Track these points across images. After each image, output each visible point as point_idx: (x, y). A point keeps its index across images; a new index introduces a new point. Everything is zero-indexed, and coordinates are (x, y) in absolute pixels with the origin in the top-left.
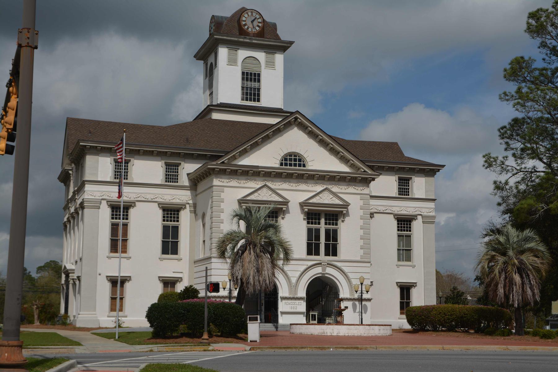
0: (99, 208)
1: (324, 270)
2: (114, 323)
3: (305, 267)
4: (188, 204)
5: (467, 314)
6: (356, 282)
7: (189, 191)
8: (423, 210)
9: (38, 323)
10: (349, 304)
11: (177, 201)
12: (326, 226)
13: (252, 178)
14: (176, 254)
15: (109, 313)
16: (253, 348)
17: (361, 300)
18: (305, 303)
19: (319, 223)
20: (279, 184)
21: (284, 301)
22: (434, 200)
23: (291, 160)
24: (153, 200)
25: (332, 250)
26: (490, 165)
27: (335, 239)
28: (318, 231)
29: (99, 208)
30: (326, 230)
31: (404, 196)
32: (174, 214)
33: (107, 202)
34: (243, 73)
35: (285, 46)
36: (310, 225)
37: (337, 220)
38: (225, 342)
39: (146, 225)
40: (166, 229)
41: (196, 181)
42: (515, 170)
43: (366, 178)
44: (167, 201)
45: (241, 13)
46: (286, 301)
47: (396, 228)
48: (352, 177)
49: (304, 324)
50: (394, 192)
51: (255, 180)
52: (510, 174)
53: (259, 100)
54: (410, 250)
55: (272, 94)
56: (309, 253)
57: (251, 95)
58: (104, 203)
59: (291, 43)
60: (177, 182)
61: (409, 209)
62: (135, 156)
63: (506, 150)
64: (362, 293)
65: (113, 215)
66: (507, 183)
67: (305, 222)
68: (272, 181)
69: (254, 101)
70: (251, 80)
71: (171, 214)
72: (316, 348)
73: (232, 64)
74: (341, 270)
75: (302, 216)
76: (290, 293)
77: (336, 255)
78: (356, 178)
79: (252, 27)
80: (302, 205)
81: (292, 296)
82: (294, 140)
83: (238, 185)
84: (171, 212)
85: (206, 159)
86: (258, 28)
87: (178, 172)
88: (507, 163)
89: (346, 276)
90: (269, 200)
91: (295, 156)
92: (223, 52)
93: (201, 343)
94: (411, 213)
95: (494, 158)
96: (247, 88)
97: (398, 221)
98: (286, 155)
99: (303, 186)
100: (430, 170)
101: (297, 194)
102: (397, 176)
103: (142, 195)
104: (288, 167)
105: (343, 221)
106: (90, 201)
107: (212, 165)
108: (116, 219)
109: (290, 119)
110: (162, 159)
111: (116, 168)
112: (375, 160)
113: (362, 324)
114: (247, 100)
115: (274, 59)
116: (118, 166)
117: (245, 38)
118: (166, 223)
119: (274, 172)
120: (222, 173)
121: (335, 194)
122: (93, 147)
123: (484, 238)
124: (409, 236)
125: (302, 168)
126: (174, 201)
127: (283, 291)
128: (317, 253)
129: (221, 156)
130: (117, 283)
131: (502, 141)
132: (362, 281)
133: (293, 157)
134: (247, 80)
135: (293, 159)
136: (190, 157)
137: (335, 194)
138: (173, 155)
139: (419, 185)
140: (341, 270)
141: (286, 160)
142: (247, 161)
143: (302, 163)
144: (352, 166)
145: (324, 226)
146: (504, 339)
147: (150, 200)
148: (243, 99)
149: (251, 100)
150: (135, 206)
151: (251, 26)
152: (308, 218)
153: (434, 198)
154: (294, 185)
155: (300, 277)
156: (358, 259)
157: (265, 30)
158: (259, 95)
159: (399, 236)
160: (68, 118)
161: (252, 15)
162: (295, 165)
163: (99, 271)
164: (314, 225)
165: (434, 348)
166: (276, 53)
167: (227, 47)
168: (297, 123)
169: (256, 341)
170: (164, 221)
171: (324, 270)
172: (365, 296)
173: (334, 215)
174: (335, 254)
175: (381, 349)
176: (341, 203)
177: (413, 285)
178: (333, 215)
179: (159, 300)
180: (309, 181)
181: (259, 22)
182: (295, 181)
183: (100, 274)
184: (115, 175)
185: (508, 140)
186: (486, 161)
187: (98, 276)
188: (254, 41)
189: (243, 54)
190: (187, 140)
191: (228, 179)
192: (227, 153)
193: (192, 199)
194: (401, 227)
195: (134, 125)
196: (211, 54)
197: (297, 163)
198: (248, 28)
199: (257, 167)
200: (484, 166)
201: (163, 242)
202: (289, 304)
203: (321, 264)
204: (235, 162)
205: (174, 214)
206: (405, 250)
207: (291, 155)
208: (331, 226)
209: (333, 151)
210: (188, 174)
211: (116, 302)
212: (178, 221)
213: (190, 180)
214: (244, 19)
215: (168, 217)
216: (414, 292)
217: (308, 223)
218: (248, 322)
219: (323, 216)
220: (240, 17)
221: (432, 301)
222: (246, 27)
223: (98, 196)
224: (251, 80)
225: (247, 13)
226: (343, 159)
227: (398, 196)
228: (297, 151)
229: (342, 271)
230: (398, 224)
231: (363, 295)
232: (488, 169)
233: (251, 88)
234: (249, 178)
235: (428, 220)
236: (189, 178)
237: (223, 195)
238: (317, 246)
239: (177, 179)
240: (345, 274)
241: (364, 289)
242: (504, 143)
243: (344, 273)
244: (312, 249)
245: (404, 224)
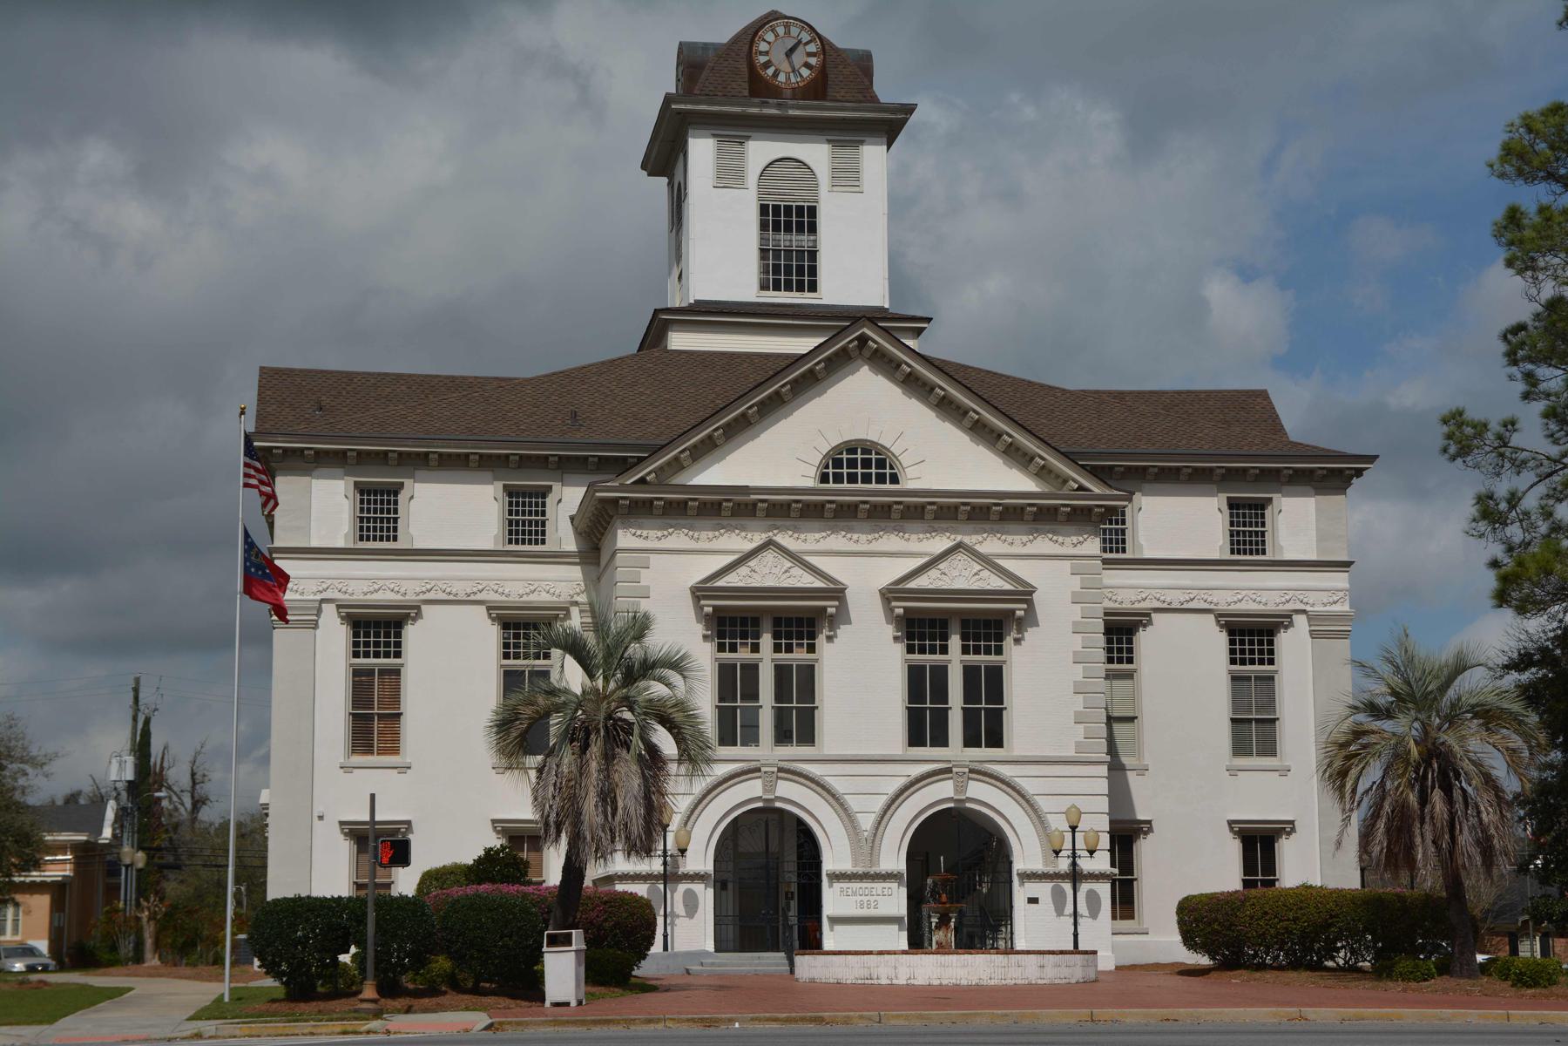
1: (960, 788)
3: (902, 782)
4: (576, 603)
5: (1336, 916)
6: (1059, 824)
7: (578, 568)
8: (1311, 597)
9: (156, 962)
10: (1043, 890)
12: (966, 657)
13: (733, 522)
16: (501, 1023)
17: (1075, 876)
18: (904, 891)
19: (944, 650)
20: (817, 536)
21: (837, 886)
22: (1348, 564)
23: (852, 464)
24: (472, 598)
25: (987, 728)
26: (1464, 451)
27: (996, 693)
28: (941, 673)
29: (316, 627)
30: (965, 668)
33: (339, 607)
34: (764, 209)
35: (891, 120)
36: (971, 657)
37: (1000, 638)
38: (467, 1009)
42: (1546, 462)
43: (1089, 509)
44: (514, 598)
45: (751, 32)
46: (845, 885)
48: (1040, 508)
49: (904, 952)
51: (743, 529)
52: (1528, 477)
53: (813, 287)
54: (1274, 721)
55: (852, 272)
56: (916, 739)
57: (788, 271)
58: (329, 611)
59: (909, 109)
60: (543, 542)
61: (1264, 597)
62: (419, 473)
63: (1526, 396)
64: (1074, 855)
65: (356, 644)
66: (1514, 499)
67: (899, 649)
68: (796, 529)
69: (800, 289)
70: (788, 225)
72: (693, 1020)
74: (1014, 788)
75: (890, 631)
76: (855, 862)
78: (1056, 508)
79: (787, 67)
80: (890, 595)
81: (860, 870)
82: (864, 405)
83: (692, 545)
85: (591, 472)
86: (805, 72)
87: (544, 513)
88: (1516, 440)
89: (1032, 806)
90: (785, 585)
91: (865, 451)
92: (702, 151)
93: (356, 1011)
94: (1271, 608)
95: (1474, 427)
96: (777, 253)
97: (1231, 633)
98: (838, 449)
99: (891, 541)
100: (1330, 474)
101: (866, 567)
102: (1223, 497)
103: (440, 584)
104: (845, 485)
105: (1017, 641)
107: (614, 488)
108: (1120, 661)
109: (860, 338)
110: (496, 479)
111: (362, 510)
112: (1152, 450)
113: (1076, 950)
114: (777, 288)
115: (857, 160)
116: (517, 504)
117: (764, 104)
118: (362, 660)
119: (797, 501)
120: (639, 511)
121: (987, 561)
122: (294, 450)
123: (1502, 677)
124: (396, 672)
125: (888, 486)
126: (533, 598)
127: (836, 855)
128: (941, 740)
129: (641, 460)
131: (1514, 369)
132: (1074, 819)
133: (859, 456)
134: (777, 228)
135: (859, 461)
136: (568, 467)
137: (987, 561)
138: (526, 463)
139: (1296, 521)
140: (1014, 788)
141: (838, 463)
142: (717, 474)
143: (888, 471)
144: (1043, 473)
145: (957, 656)
146: (1404, 990)
147: (462, 597)
148: (764, 286)
149: (789, 288)
150: (1150, 622)
151: (785, 66)
152: (910, 636)
153: (1343, 557)
154: (863, 537)
155: (885, 812)
156: (1070, 753)
157: (831, 76)
158: (813, 271)
159: (1236, 679)
160: (262, 369)
161: (788, 33)
162: (867, 479)
164: (927, 656)
165: (1409, 1016)
166: (862, 142)
167: (714, 136)
168: (867, 353)
169: (567, 1004)
170: (506, 656)
171: (770, 787)
172: (1086, 865)
173: (992, 624)
174: (996, 740)
175: (893, 1022)
176: (1008, 587)
177: (1285, 828)
178: (987, 624)
179: (420, 888)
180: (908, 525)
181: (810, 54)
182: (659, 522)
183: (321, 818)
184: (361, 529)
185: (1530, 367)
186: (1449, 436)
188: (791, 112)
189: (761, 151)
190: (574, 415)
191: (820, 531)
192: (656, 450)
193: (587, 590)
194: (1243, 652)
195: (453, 379)
196: (676, 160)
197: (873, 471)
198: (776, 74)
199: (745, 490)
200: (1445, 450)
201: (355, 717)
202: (854, 894)
203: (949, 771)
204: (679, 479)
206: (1257, 721)
207: (853, 451)
208: (982, 657)
209: (980, 431)
210: (572, 518)
212: (1271, 662)
213: (579, 533)
214: (763, 47)
215: (517, 646)
216: (1286, 850)
217: (910, 650)
218: (545, 949)
219: (767, 624)
220: (752, 42)
221: (1347, 877)
222: (770, 71)
224: (788, 225)
225: (773, 30)
226: (1016, 456)
227: (1227, 556)
228: (872, 436)
229: (1019, 792)
230: (1232, 642)
231: (1078, 861)
232: (1459, 460)
233: (789, 252)
234: (725, 522)
235: (1324, 628)
236: (575, 529)
237: (646, 577)
238: (941, 718)
239: (544, 533)
240: (1028, 801)
241: (1080, 844)
242: (1519, 376)
243: (1023, 796)
244: (924, 727)
245: (1251, 643)
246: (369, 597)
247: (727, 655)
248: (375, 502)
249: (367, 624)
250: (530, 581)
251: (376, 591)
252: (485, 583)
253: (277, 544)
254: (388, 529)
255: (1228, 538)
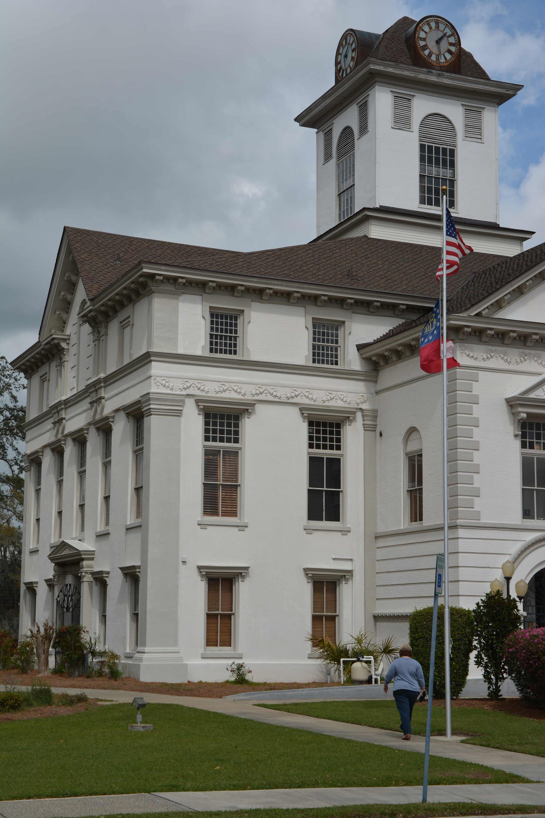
0: (178, 414)
2: (230, 673)
11: (338, 404)
13: (533, 352)
14: (234, 514)
15: (205, 650)
24: (291, 401)
31: (223, 356)
32: (331, 433)
33: (197, 402)
34: (422, 147)
39: (275, 455)
40: (315, 463)
41: (377, 361)
44: (319, 403)
47: (305, 441)
50: (300, 351)
54: (236, 486)
59: (517, 88)
70: (437, 160)
71: (325, 432)
73: (401, 126)
77: (337, 519)
83: (505, 366)
84: (325, 429)
86: (448, 56)
87: (337, 342)
96: (430, 178)
97: (311, 424)
103: (268, 388)
106: (162, 399)
111: (212, 329)
118: (315, 450)
120: (479, 335)
130: (221, 583)
136: (366, 308)
147: (284, 399)
148: (422, 202)
151: (435, 50)
161: (437, 27)
163: (183, 555)
181: (451, 44)
183: (184, 562)
187: (182, 567)
189: (423, 106)
204: (501, 315)
205: (331, 433)
210: (360, 347)
211: (220, 628)
214: (422, 35)
222: (427, 52)
223: (177, 388)
224: (437, 160)
227: (207, 354)
230: (207, 423)
233: (437, 179)
234: (527, 351)
237: (477, 389)
246: (219, 395)
247: (528, 451)
248: (222, 324)
249: (215, 416)
250: (330, 391)
251: (224, 391)
252: (299, 391)
253: (155, 349)
254: (230, 345)
255: (311, 351)
